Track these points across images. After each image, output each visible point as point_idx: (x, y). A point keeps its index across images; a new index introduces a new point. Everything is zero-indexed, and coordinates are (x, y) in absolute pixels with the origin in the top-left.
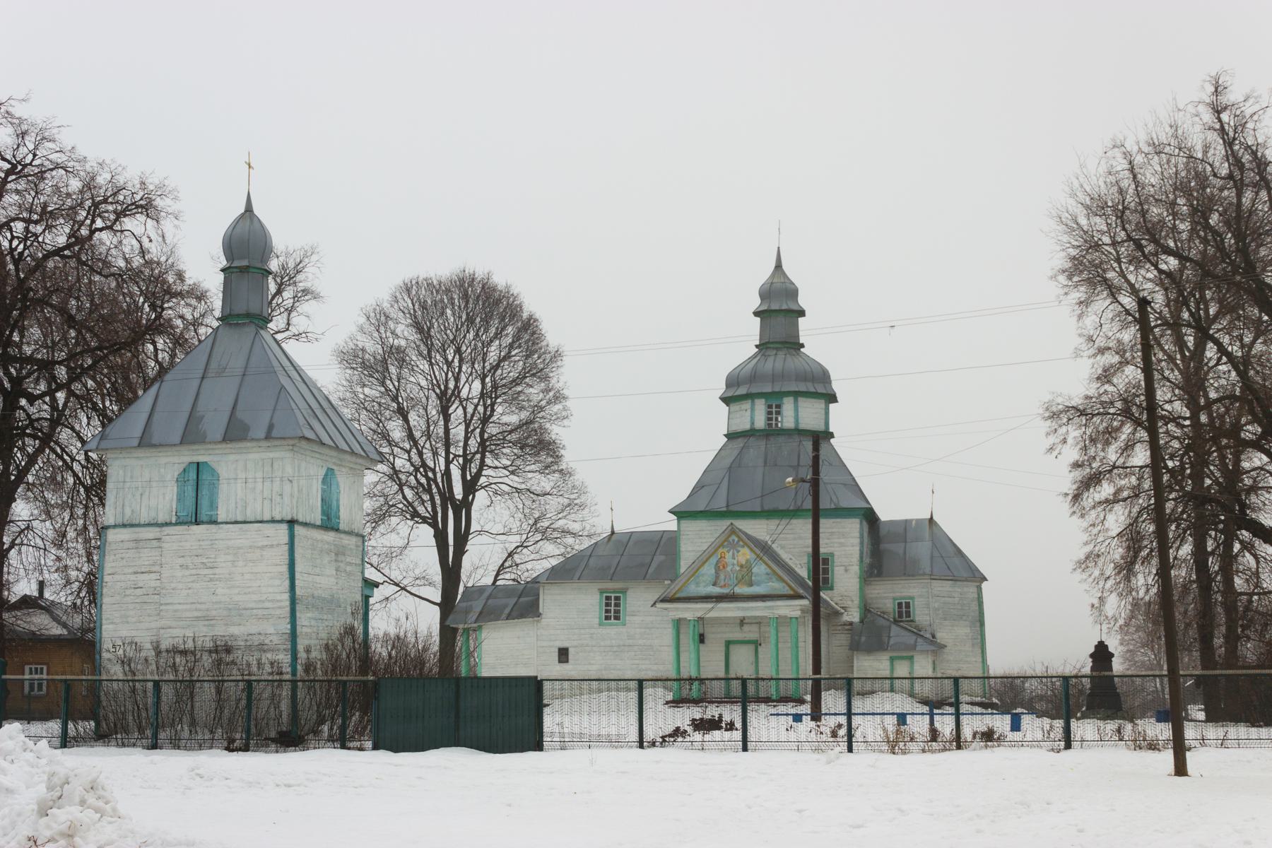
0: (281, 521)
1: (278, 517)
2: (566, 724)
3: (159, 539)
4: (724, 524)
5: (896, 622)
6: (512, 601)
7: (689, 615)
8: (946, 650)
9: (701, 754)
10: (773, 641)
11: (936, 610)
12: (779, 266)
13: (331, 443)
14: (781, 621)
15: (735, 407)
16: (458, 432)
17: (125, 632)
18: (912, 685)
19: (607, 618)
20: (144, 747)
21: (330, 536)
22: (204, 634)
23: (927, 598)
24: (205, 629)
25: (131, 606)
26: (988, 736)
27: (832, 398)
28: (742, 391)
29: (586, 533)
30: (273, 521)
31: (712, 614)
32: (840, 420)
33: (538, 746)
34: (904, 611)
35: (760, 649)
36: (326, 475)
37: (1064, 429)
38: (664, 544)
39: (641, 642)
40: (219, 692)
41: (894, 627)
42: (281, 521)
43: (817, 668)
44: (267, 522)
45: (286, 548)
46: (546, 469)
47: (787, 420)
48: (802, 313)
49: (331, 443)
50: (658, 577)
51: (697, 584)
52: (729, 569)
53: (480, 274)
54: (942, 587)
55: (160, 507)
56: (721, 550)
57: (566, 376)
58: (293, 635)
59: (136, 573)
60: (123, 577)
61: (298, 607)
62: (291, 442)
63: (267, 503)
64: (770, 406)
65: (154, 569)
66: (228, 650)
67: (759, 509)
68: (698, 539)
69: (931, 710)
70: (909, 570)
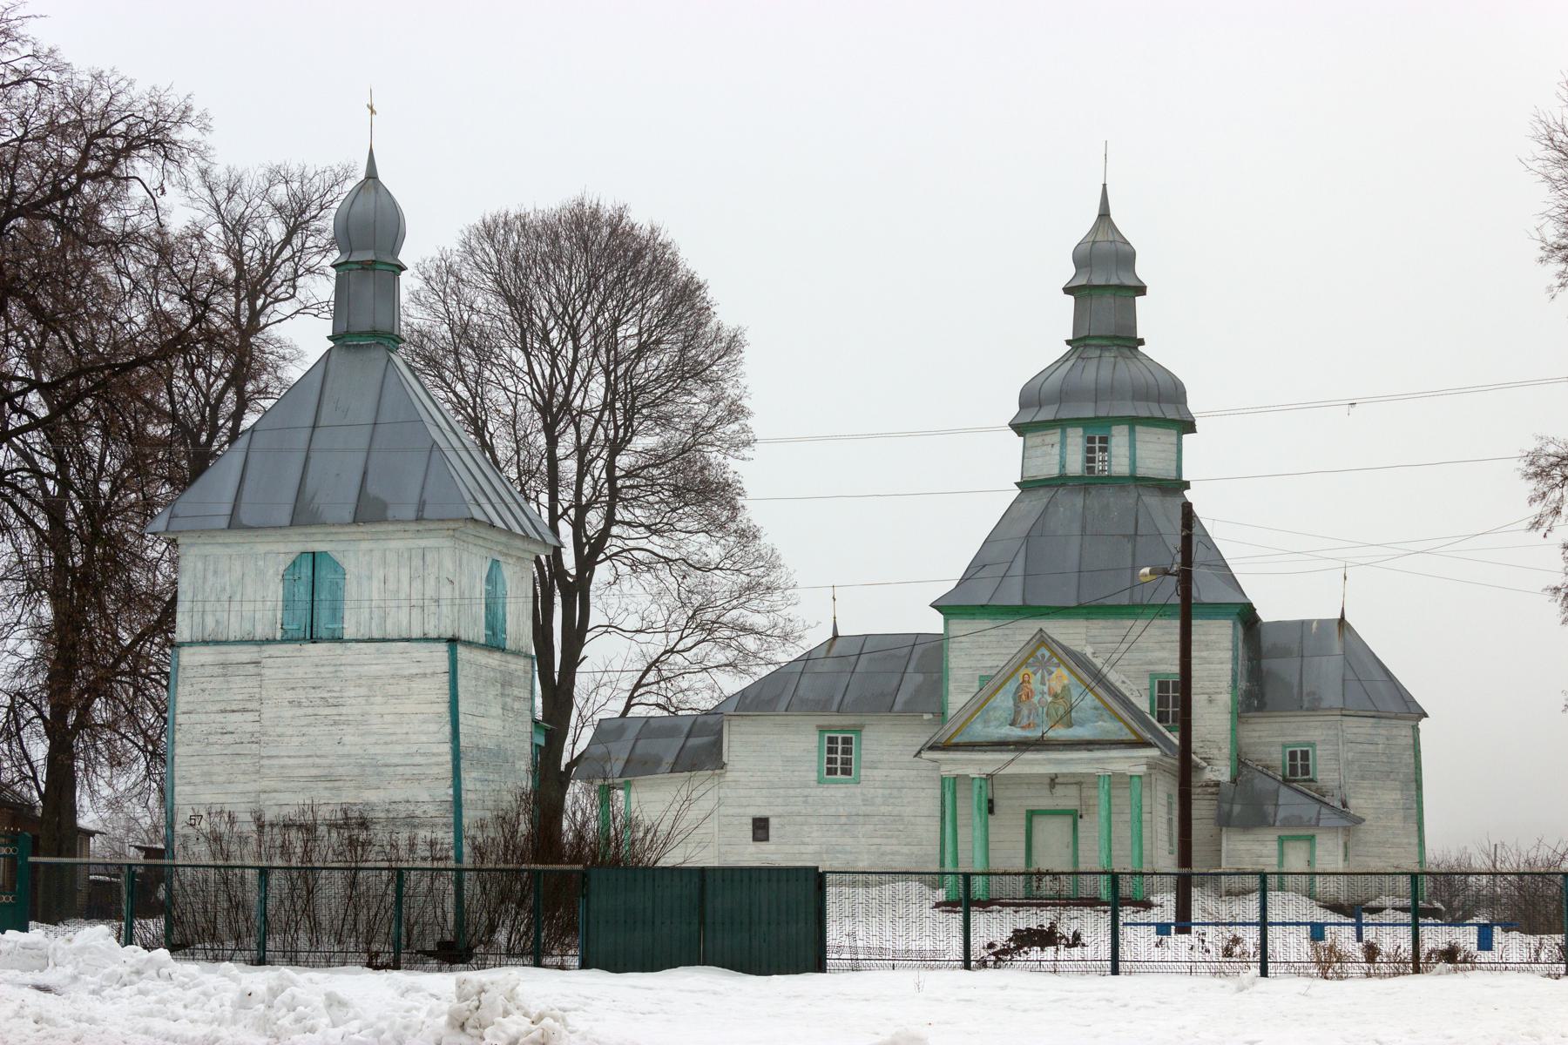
0: (438, 640)
1: (433, 634)
2: (860, 934)
3: (257, 663)
4: (1027, 629)
5: (1286, 781)
6: (678, 743)
7: (972, 771)
8: (1362, 827)
9: (1054, 977)
10: (1104, 813)
11: (1349, 763)
12: (1104, 214)
13: (519, 532)
14: (1117, 781)
15: (1035, 439)
16: (569, 468)
17: (208, 796)
18: (1312, 883)
19: (831, 772)
20: (245, 962)
21: (494, 660)
22: (328, 802)
23: (1333, 745)
24: (327, 794)
25: (217, 760)
26: (1450, 955)
27: (1189, 427)
28: (1046, 414)
29: (777, 632)
30: (426, 639)
31: (1009, 770)
32: (1200, 460)
33: (819, 966)
34: (1299, 765)
35: (1080, 823)
36: (491, 569)
37: (1557, 493)
38: (924, 656)
39: (884, 809)
40: (353, 884)
41: (1284, 791)
42: (438, 640)
43: (1185, 857)
44: (417, 640)
45: (446, 678)
46: (715, 526)
47: (1119, 462)
48: (1141, 290)
49: (519, 532)
50: (911, 710)
51: (986, 722)
52: (1035, 699)
53: (608, 208)
54: (1359, 728)
55: (258, 615)
56: (1023, 671)
57: (756, 378)
58: (457, 803)
59: (225, 711)
60: (204, 718)
61: (464, 764)
62: (452, 525)
63: (416, 612)
64: (1091, 440)
65: (249, 706)
66: (364, 824)
67: (1074, 604)
68: (980, 652)
69: (1415, 919)
70: (1306, 704)
